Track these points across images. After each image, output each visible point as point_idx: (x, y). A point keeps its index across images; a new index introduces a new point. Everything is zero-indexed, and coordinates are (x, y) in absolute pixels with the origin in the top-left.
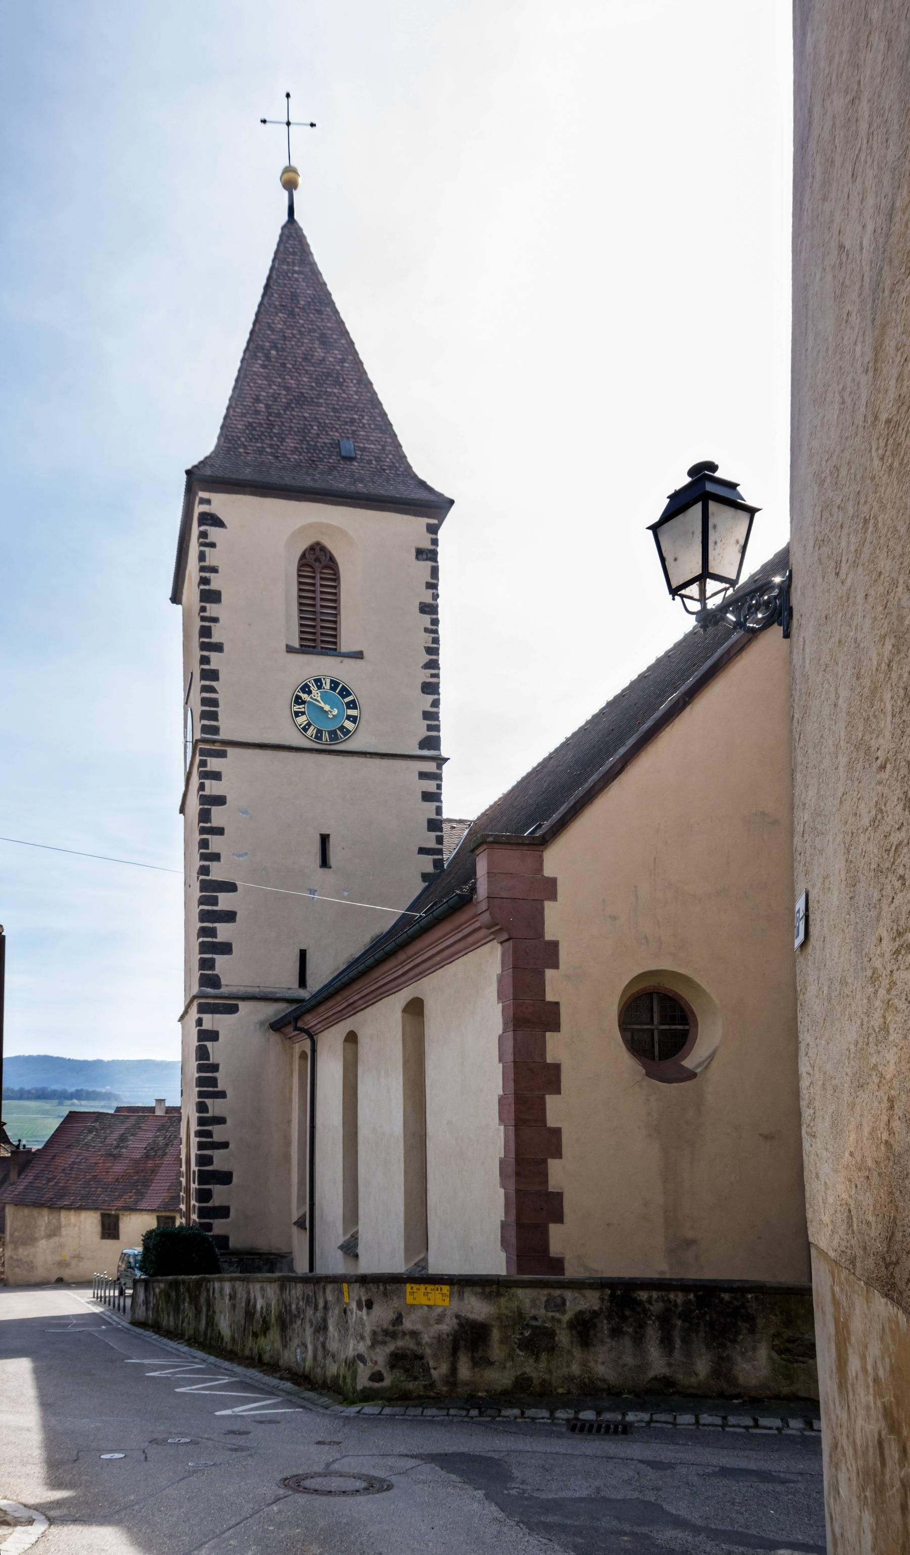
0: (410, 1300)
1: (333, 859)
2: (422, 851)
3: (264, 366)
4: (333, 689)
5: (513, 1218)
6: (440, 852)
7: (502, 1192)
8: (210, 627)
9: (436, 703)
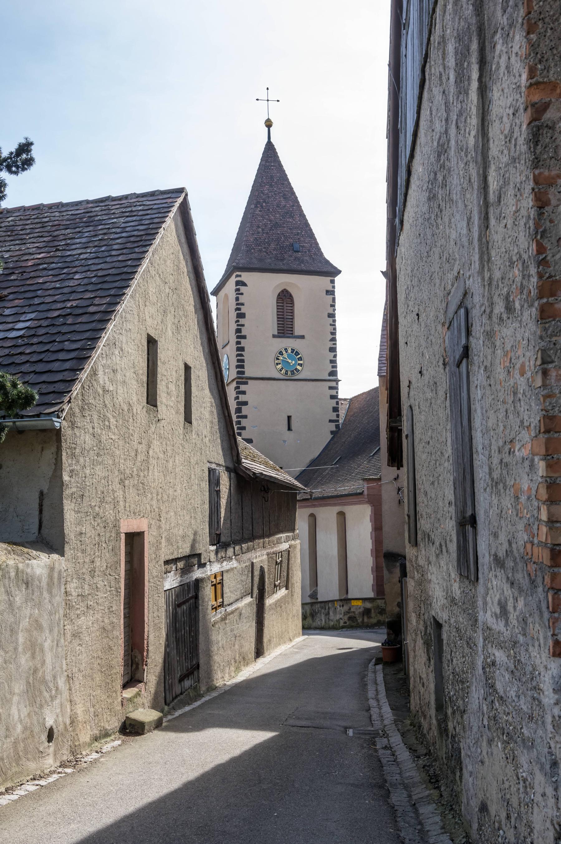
0: (352, 604)
1: (293, 427)
2: (331, 421)
3: (260, 211)
4: (292, 352)
5: (375, 583)
6: (338, 421)
7: (372, 576)
8: (241, 329)
9: (335, 356)
